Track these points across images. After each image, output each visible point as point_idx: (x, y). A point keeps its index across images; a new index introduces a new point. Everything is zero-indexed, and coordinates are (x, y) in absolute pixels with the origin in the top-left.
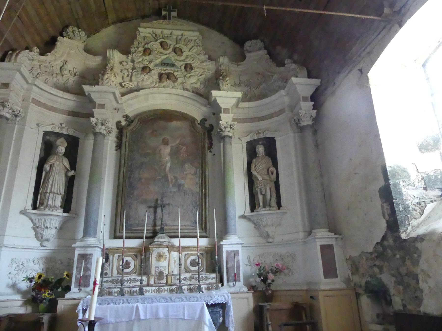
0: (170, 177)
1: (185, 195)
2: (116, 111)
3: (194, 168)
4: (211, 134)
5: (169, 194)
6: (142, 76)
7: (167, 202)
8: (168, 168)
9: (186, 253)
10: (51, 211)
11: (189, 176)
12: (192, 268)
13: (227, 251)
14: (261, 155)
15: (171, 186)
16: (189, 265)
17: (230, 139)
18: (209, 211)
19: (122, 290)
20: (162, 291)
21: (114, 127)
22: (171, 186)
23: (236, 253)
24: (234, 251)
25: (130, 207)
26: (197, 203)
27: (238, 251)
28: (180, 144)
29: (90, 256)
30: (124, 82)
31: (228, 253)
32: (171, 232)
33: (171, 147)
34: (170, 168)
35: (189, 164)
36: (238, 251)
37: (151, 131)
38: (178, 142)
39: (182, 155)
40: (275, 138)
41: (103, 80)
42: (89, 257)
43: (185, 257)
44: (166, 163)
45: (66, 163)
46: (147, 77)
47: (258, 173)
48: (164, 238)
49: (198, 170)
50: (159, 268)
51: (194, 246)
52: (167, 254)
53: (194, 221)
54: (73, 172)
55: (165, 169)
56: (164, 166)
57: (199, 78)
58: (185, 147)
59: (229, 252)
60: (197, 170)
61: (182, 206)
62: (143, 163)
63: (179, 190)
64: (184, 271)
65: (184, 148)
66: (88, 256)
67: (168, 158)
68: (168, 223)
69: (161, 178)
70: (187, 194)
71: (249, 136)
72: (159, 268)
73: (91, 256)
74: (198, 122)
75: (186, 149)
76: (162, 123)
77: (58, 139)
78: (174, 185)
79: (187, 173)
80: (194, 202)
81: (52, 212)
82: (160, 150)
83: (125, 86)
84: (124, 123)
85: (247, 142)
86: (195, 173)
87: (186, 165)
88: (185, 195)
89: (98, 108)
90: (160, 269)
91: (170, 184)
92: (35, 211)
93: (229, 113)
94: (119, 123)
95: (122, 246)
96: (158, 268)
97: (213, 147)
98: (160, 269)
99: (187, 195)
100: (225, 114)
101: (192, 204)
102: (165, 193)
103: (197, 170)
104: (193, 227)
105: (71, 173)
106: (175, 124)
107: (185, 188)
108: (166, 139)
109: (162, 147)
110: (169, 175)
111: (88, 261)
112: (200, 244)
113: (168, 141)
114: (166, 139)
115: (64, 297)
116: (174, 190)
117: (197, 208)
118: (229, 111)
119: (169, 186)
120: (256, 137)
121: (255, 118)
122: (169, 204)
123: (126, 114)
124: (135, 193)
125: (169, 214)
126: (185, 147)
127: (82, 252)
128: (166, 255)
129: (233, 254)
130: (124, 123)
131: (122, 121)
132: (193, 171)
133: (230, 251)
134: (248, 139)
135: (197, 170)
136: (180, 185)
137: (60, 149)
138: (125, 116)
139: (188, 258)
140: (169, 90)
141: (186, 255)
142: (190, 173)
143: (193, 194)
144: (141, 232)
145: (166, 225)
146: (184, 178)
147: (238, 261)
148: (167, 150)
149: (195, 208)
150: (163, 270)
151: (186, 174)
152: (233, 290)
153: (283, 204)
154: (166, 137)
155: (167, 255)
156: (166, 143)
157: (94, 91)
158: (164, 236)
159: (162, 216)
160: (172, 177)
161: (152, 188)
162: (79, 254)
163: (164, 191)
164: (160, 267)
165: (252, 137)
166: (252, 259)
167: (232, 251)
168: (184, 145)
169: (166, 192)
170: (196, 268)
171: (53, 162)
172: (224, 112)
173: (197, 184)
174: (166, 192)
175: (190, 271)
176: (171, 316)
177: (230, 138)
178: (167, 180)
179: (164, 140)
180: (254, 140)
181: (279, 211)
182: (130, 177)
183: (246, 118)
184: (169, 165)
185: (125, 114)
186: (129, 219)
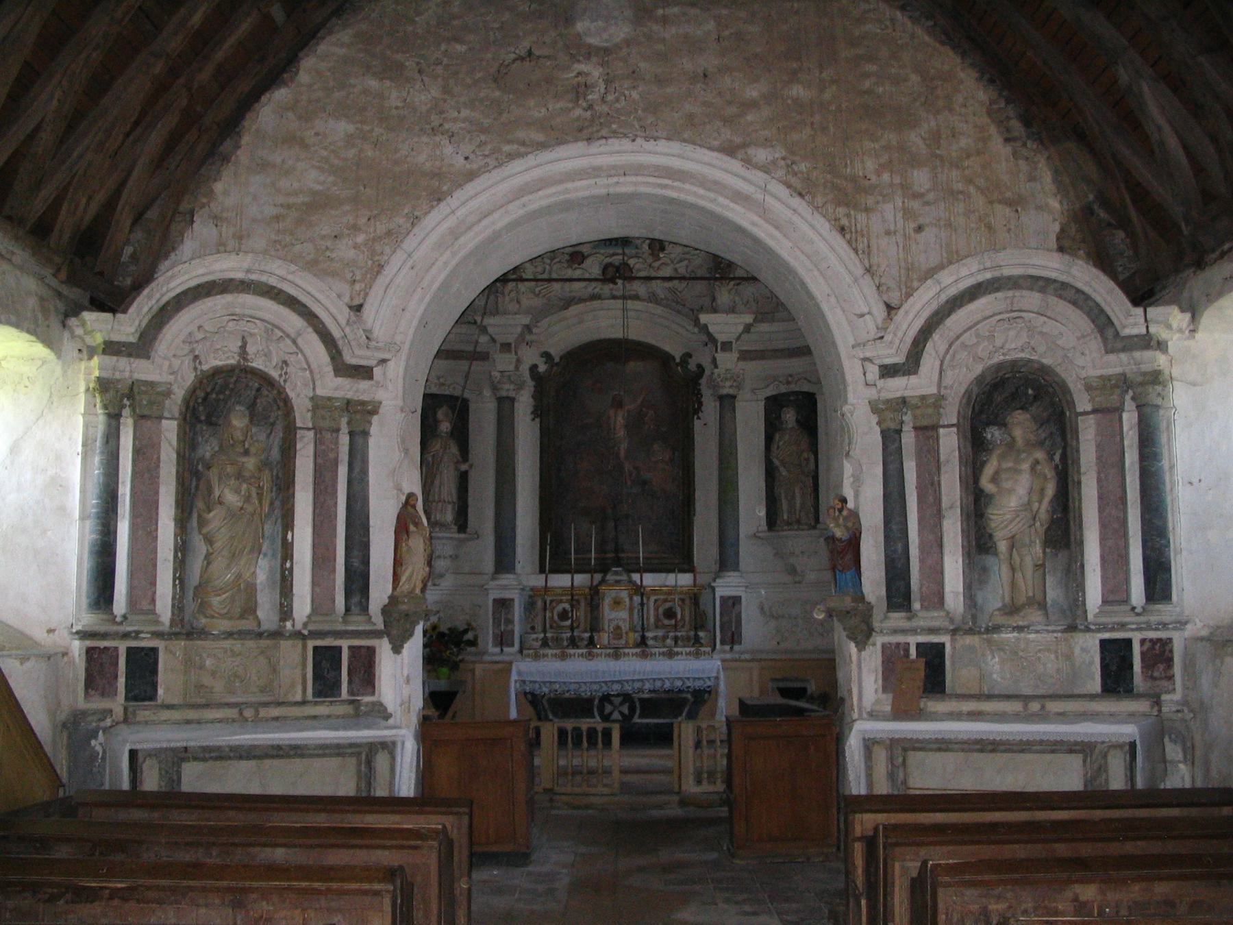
0: (628, 467)
4: (700, 384)
9: (655, 597)
12: (666, 622)
13: (721, 597)
14: (790, 426)
15: (629, 483)
19: (643, 638)
20: (620, 656)
22: (629, 483)
23: (736, 600)
31: (724, 600)
33: (629, 411)
38: (639, 402)
41: (503, 294)
45: (454, 449)
52: (627, 600)
57: (677, 266)
65: (651, 412)
67: (621, 433)
71: (771, 387)
84: (542, 368)
94: (534, 368)
97: (703, 408)
106: (634, 366)
112: (680, 583)
115: (152, 697)
120: (783, 389)
121: (782, 350)
123: (546, 349)
127: (498, 596)
129: (730, 602)
130: (542, 368)
134: (770, 392)
136: (645, 483)
141: (656, 601)
145: (623, 551)
148: (619, 419)
150: (621, 624)
152: (728, 656)
156: (618, 404)
162: (494, 600)
166: (766, 608)
167: (729, 598)
175: (665, 626)
176: (618, 582)
184: (624, 446)
185: (543, 350)
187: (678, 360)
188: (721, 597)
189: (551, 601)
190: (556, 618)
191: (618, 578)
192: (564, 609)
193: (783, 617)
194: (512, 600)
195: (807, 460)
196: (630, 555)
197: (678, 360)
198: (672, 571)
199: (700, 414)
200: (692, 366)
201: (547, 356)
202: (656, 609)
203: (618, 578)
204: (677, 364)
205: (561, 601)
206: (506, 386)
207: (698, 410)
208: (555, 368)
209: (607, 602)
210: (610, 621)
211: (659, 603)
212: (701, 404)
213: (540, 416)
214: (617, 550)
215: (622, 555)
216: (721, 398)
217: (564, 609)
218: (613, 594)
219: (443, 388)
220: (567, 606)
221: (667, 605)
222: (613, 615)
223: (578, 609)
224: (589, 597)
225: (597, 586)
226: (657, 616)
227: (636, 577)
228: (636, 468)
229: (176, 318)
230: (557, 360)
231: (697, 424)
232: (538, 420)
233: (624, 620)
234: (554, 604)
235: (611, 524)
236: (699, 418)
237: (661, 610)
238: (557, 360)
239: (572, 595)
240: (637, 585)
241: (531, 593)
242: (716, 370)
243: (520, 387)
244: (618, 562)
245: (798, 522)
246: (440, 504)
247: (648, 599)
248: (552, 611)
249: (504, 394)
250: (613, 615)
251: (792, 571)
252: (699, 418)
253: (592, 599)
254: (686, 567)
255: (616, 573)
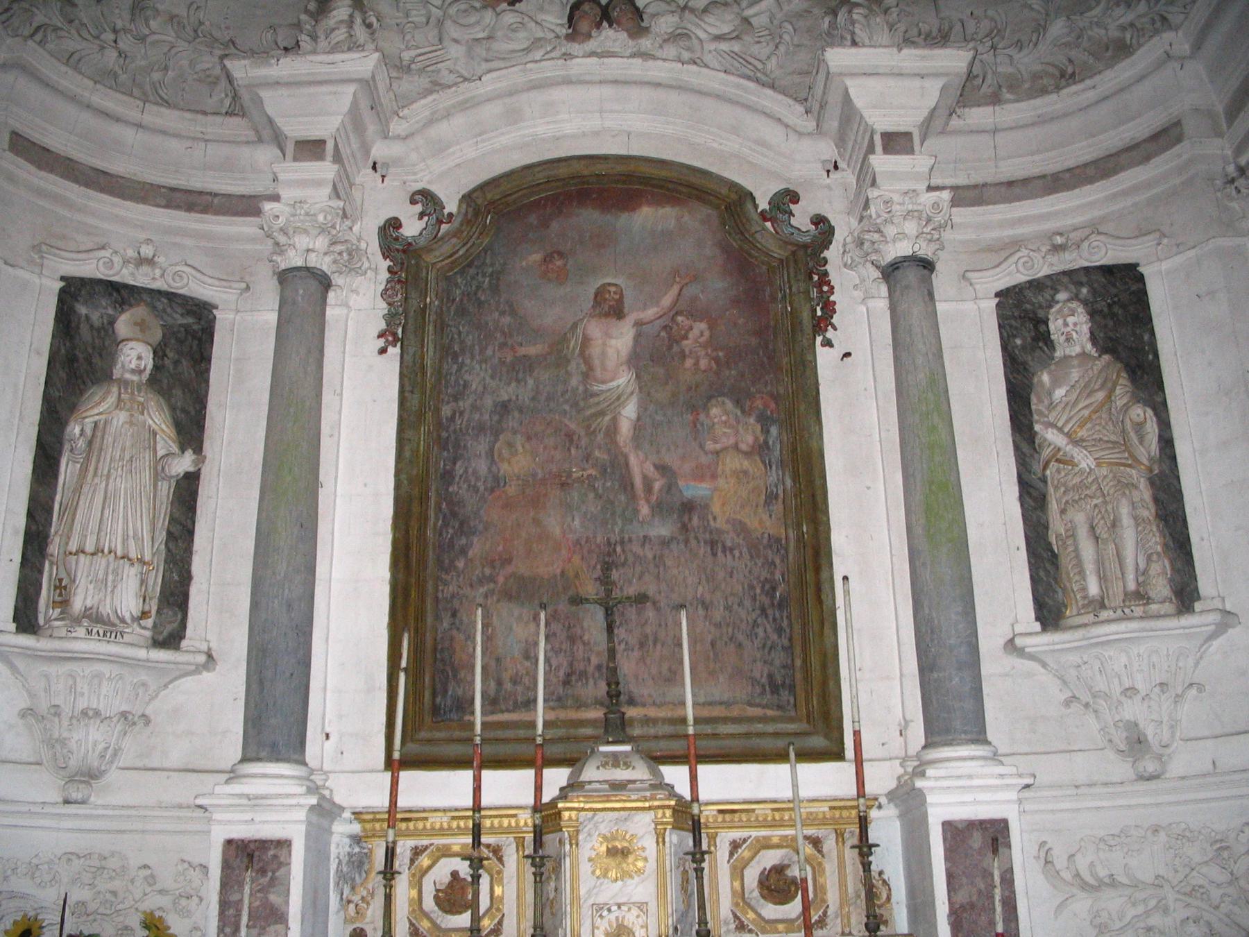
0: (639, 466)
1: (714, 555)
2: (378, 176)
3: (752, 420)
4: (825, 261)
5: (639, 551)
6: (488, 16)
7: (631, 591)
8: (625, 427)
9: (737, 834)
10: (96, 637)
11: (732, 462)
12: (771, 911)
13: (947, 826)
15: (645, 510)
16: (756, 893)
17: (926, 272)
18: (80, 830)
21: (372, 244)
22: (645, 510)
24: (982, 822)
25: (454, 615)
26: (774, 589)
27: (1005, 822)
28: (675, 311)
29: (282, 854)
30: (408, 48)
31: (956, 833)
32: (656, 737)
33: (638, 324)
34: (638, 426)
35: (729, 405)
36: (1005, 822)
37: (537, 257)
38: (667, 301)
39: (689, 363)
40: (1137, 265)
42: (275, 857)
43: (731, 854)
44: (619, 400)
45: (158, 419)
46: (509, 18)
47: (1068, 435)
48: (627, 765)
49: (774, 430)
50: (609, 910)
51: (775, 802)
53: (764, 680)
54: (189, 456)
55: (613, 429)
56: (607, 418)
58: (703, 326)
59: (956, 828)
60: (766, 431)
61: (706, 607)
62: (504, 408)
63: (685, 528)
64: (733, 926)
66: (271, 853)
67: (623, 379)
68: (636, 690)
69: (594, 473)
70: (724, 547)
72: (609, 910)
73: (284, 851)
74: (756, 206)
75: (707, 334)
76: (588, 217)
77: (123, 311)
78: (659, 509)
79: (718, 447)
80: (763, 587)
81: (104, 644)
82: (586, 341)
83: (413, 66)
84: (412, 228)
85: (997, 295)
86: (761, 449)
87: (714, 411)
88: (714, 555)
89: (295, 159)
90: (617, 918)
91: (642, 502)
92: (26, 640)
93: (910, 151)
95: (387, 804)
96: (605, 913)
97: (835, 320)
98: (624, 917)
99: (724, 551)
100: (890, 157)
101: (754, 599)
102: (619, 549)
103: (768, 432)
104: (764, 707)
105: (183, 464)
107: (715, 518)
108: (613, 289)
109: (595, 329)
110: (633, 460)
111: (270, 874)
113: (620, 301)
114: (613, 289)
116: (662, 529)
117: (777, 615)
118: (911, 140)
119: (636, 511)
120: (1043, 270)
121: (1025, 181)
122: (641, 599)
124: (478, 548)
125: (642, 645)
126: (703, 326)
128: (644, 849)
131: (402, 219)
132: (749, 435)
133: (962, 821)
134: (1012, 275)
135: (766, 431)
136: (688, 507)
137: (134, 354)
138: (418, 197)
139: (746, 863)
140: (614, 66)
141: (735, 846)
142: (736, 447)
143: (754, 549)
144: (500, 734)
145: (632, 702)
146: (705, 473)
147: (1006, 871)
149: (767, 617)
151: (717, 453)
153: (1205, 585)
154: (613, 281)
155: (646, 845)
157: (278, 83)
158: (625, 754)
159: (612, 653)
160: (650, 470)
161: (553, 523)
163: (615, 538)
164: (614, 908)
165: (1021, 269)
167: (972, 825)
168: (695, 313)
169: (622, 542)
170: (794, 908)
171: (101, 413)
172: (887, 150)
173: (771, 498)
174: (622, 542)
177: (925, 267)
178: (626, 485)
179: (599, 295)
180: (1036, 285)
181: (1187, 620)
182: (448, 477)
183: (985, 185)
184: (630, 411)
186: (455, 676)
187: (763, 205)
188: (947, 826)
189: (417, 852)
190: (429, 903)
191: (621, 774)
192: (455, 875)
193: (1113, 883)
194: (284, 844)
195: (1139, 426)
196: (652, 712)
197: (763, 205)
198: (779, 757)
199: (830, 334)
200: (801, 218)
201: (426, 199)
202: (738, 872)
203: (621, 774)
204: (764, 216)
205: (446, 852)
206: (302, 241)
207: (823, 322)
208: (444, 227)
209: (591, 846)
210: (599, 908)
211: (744, 852)
212: (829, 308)
213: (403, 342)
214: (614, 696)
215: (631, 712)
216: (891, 272)
217: (455, 875)
218: (605, 824)
219: (145, 269)
220: (464, 868)
221: (770, 858)
222: (610, 891)
223: (496, 878)
224: (529, 837)
225: (553, 803)
226: (740, 896)
227: (676, 776)
228: (662, 469)
229: (18, 573)
230: (451, 207)
231: (825, 359)
232: (394, 351)
233: (642, 906)
234: (425, 861)
235: (593, 621)
236: (828, 343)
237: (752, 876)
238: (451, 207)
239: (477, 832)
240: (680, 798)
241: (356, 828)
242: (873, 193)
243: (351, 259)
244: (616, 728)
245: (1140, 596)
246: (101, 562)
247: (713, 839)
248: (417, 881)
249: (294, 259)
250: (610, 891)
251: (1137, 743)
252: (828, 343)
253: (538, 842)
254: (818, 742)
255: (615, 761)
